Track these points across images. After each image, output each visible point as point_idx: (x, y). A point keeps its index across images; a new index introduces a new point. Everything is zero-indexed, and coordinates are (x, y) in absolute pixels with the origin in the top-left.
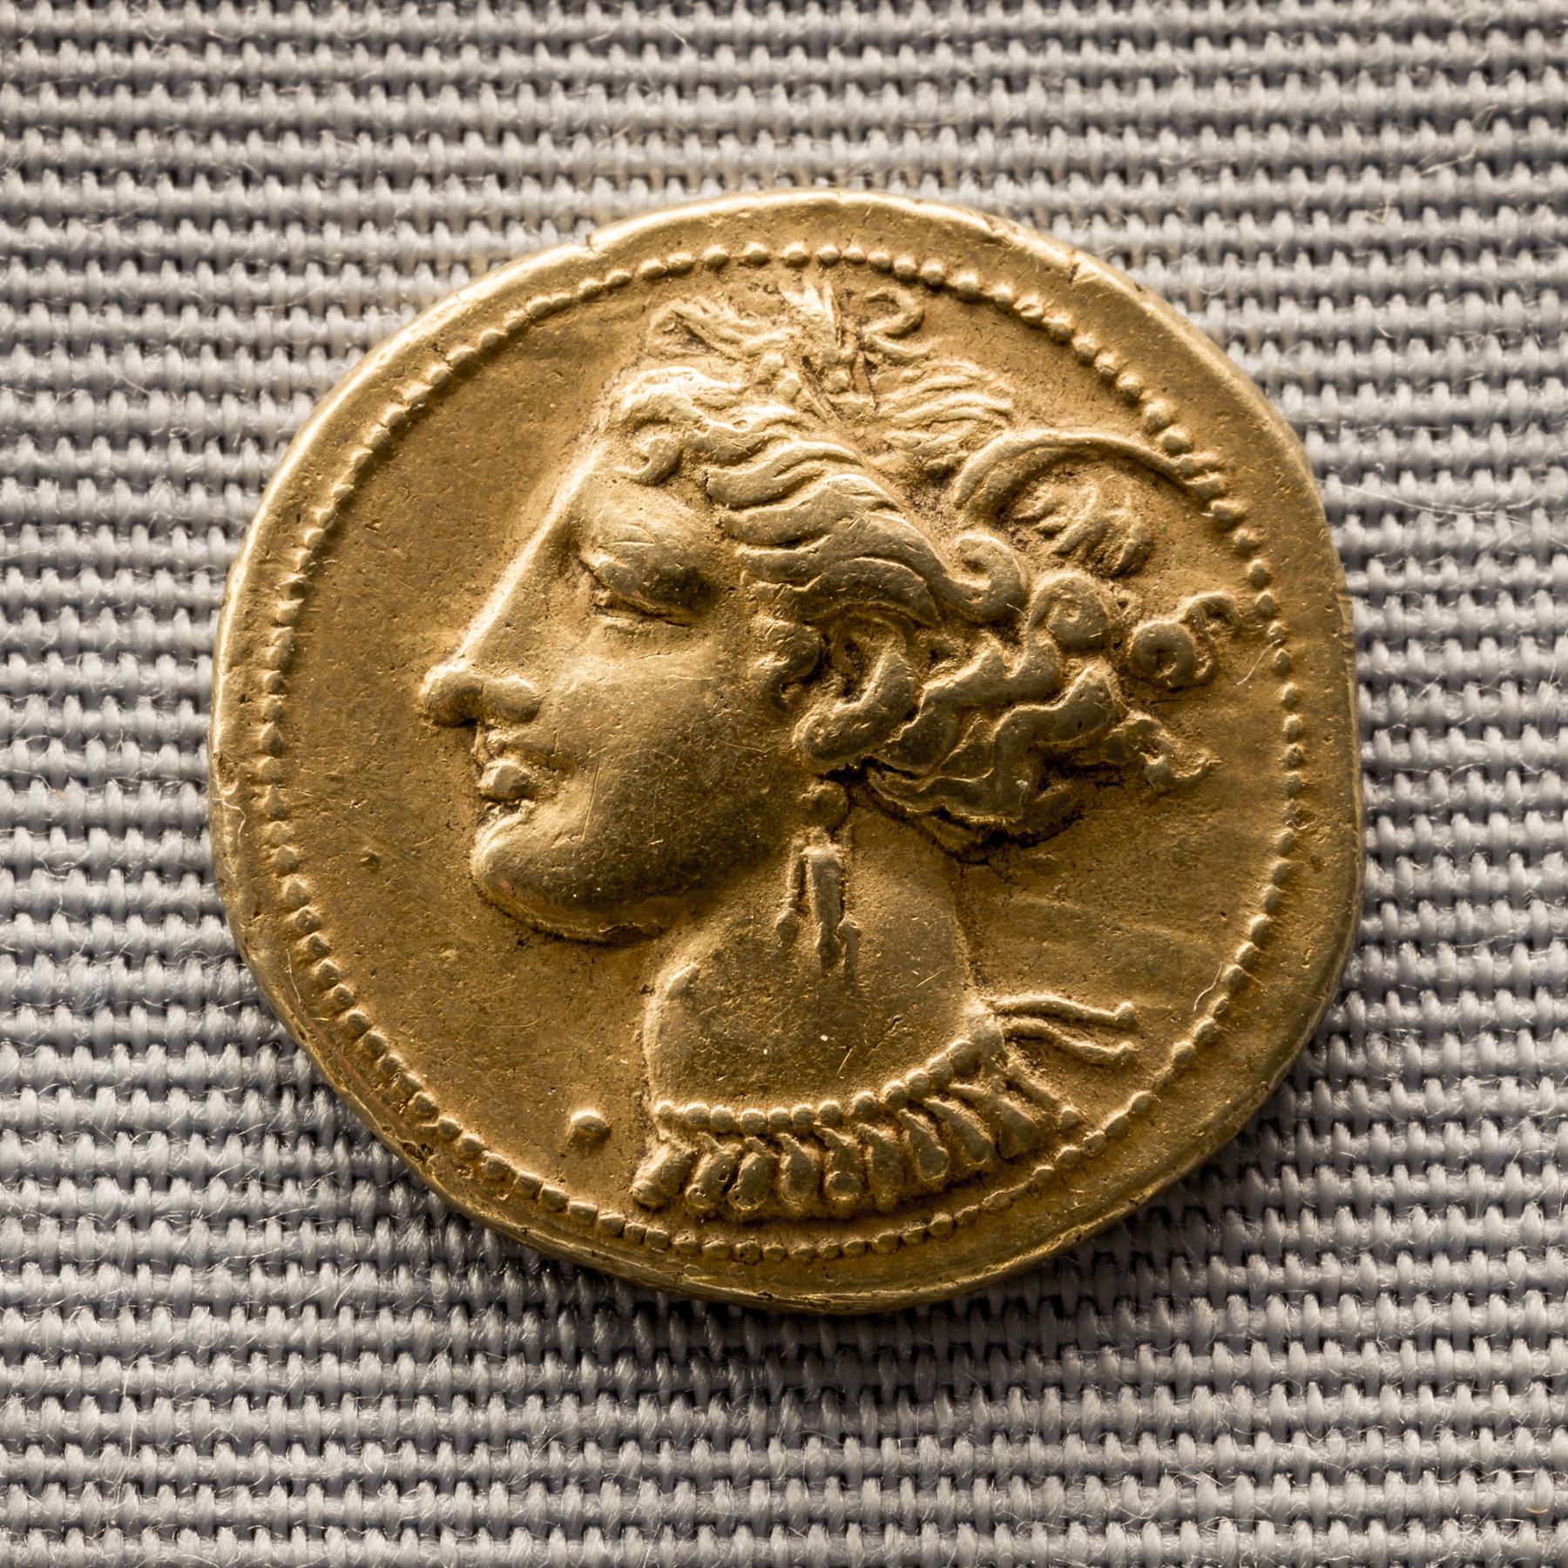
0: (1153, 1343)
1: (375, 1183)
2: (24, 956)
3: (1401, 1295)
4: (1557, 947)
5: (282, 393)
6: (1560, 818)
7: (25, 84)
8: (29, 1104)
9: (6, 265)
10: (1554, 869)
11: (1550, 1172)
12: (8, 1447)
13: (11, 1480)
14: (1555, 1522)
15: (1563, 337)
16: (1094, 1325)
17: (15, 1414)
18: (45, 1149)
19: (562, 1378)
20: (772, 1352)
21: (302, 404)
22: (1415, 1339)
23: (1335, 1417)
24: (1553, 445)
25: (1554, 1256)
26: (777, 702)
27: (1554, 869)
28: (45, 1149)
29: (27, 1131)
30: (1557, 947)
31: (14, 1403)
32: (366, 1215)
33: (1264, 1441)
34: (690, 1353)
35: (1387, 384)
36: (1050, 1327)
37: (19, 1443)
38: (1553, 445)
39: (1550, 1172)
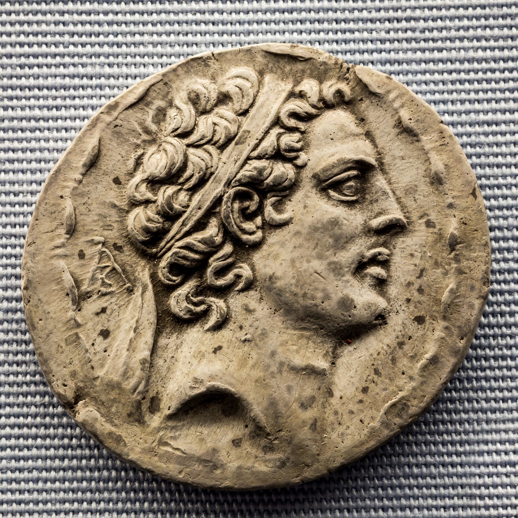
2: (5, 247)
4: (515, 252)
6: (515, 178)
7: (5, 130)
8: (7, 144)
9: (1, 217)
12: (2, 205)
13: (2, 213)
15: (516, 315)
16: (329, 495)
17: (3, 198)
18: (11, 155)
24: (514, 405)
28: (11, 155)
29: (6, 150)
31: (3, 195)
32: (94, 490)
33: (392, 33)
37: (4, 205)
38: (514, 405)
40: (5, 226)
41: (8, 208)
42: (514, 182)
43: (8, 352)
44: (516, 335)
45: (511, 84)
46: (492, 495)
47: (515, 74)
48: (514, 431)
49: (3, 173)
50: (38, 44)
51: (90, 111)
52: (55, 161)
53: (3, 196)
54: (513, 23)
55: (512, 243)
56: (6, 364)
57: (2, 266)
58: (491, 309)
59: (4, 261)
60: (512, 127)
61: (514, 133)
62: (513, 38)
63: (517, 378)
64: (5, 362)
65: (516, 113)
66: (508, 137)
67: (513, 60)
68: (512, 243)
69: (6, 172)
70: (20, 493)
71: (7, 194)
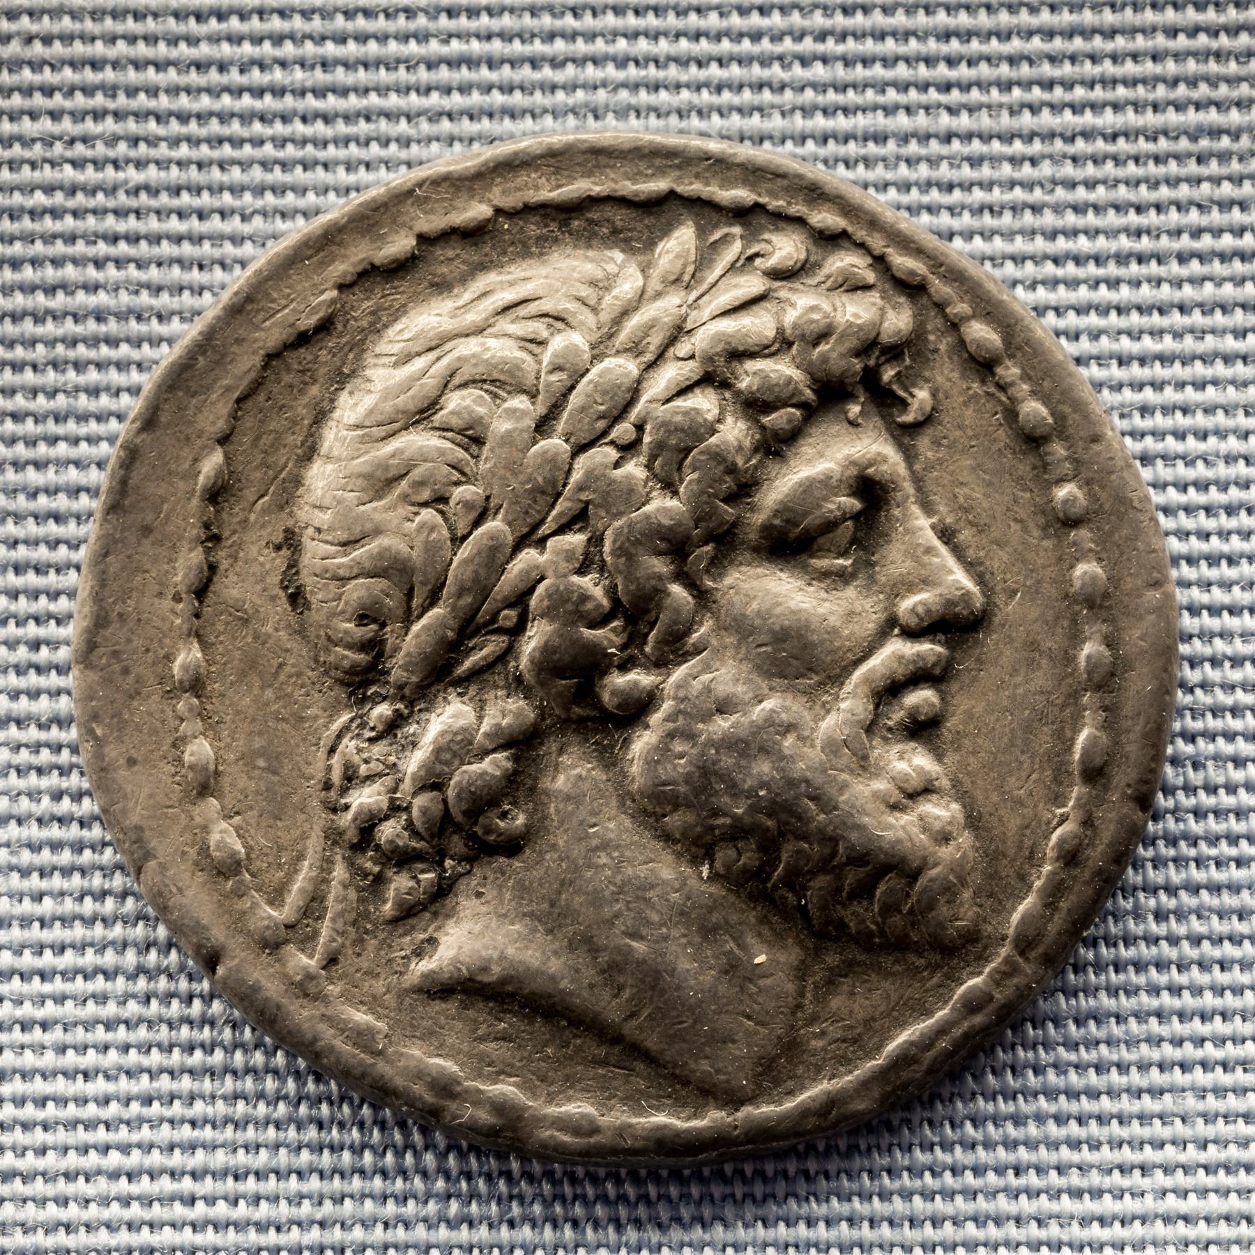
0: (860, 1195)
1: (220, 996)
3: (1060, 1119)
5: (155, 341)
9: (1, 422)
10: (1249, 998)
11: (1245, 894)
14: (1249, 107)
15: (1249, 764)
19: (311, 1163)
20: (603, 1198)
21: (165, 348)
22: (1090, 1192)
23: (929, 1214)
25: (1248, 994)
26: (341, 373)
27: (1246, 570)
30: (1249, 1043)
34: (555, 1197)
35: (1073, 284)
36: (802, 1188)
38: (1247, 1029)
39: (1244, 843)
40: (14, 544)
41: (20, 450)
42: (1245, 547)
43: (17, 748)
44: (1252, 912)
45: (1239, 318)
46: (1195, 555)
47: (1248, 241)
48: (1247, 1117)
49: (6, 268)
50: (94, 162)
51: (218, 274)
52: (134, 391)
53: (8, 373)
54: (1243, 71)
55: (1241, 697)
56: (16, 978)
57: (8, 845)
58: (1192, 801)
59: (12, 579)
60: (1240, 1077)
61: (1246, 485)
62: (1243, 206)
63: (1252, 912)
64: (11, 868)
65: (1250, 1094)
66: (1232, 1102)
67: (1244, 257)
68: (1241, 697)
69: (16, 264)
70: (47, 1232)
71: (16, 317)
